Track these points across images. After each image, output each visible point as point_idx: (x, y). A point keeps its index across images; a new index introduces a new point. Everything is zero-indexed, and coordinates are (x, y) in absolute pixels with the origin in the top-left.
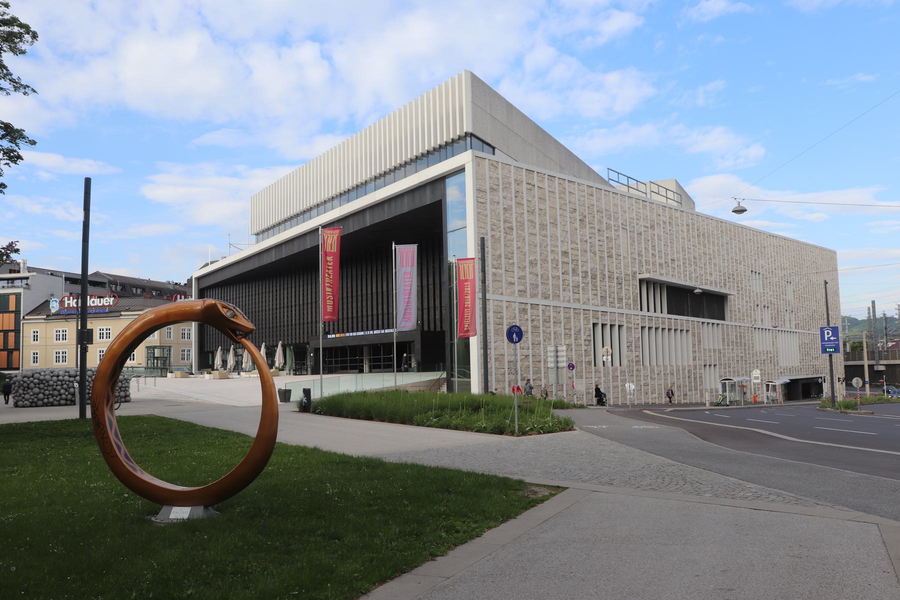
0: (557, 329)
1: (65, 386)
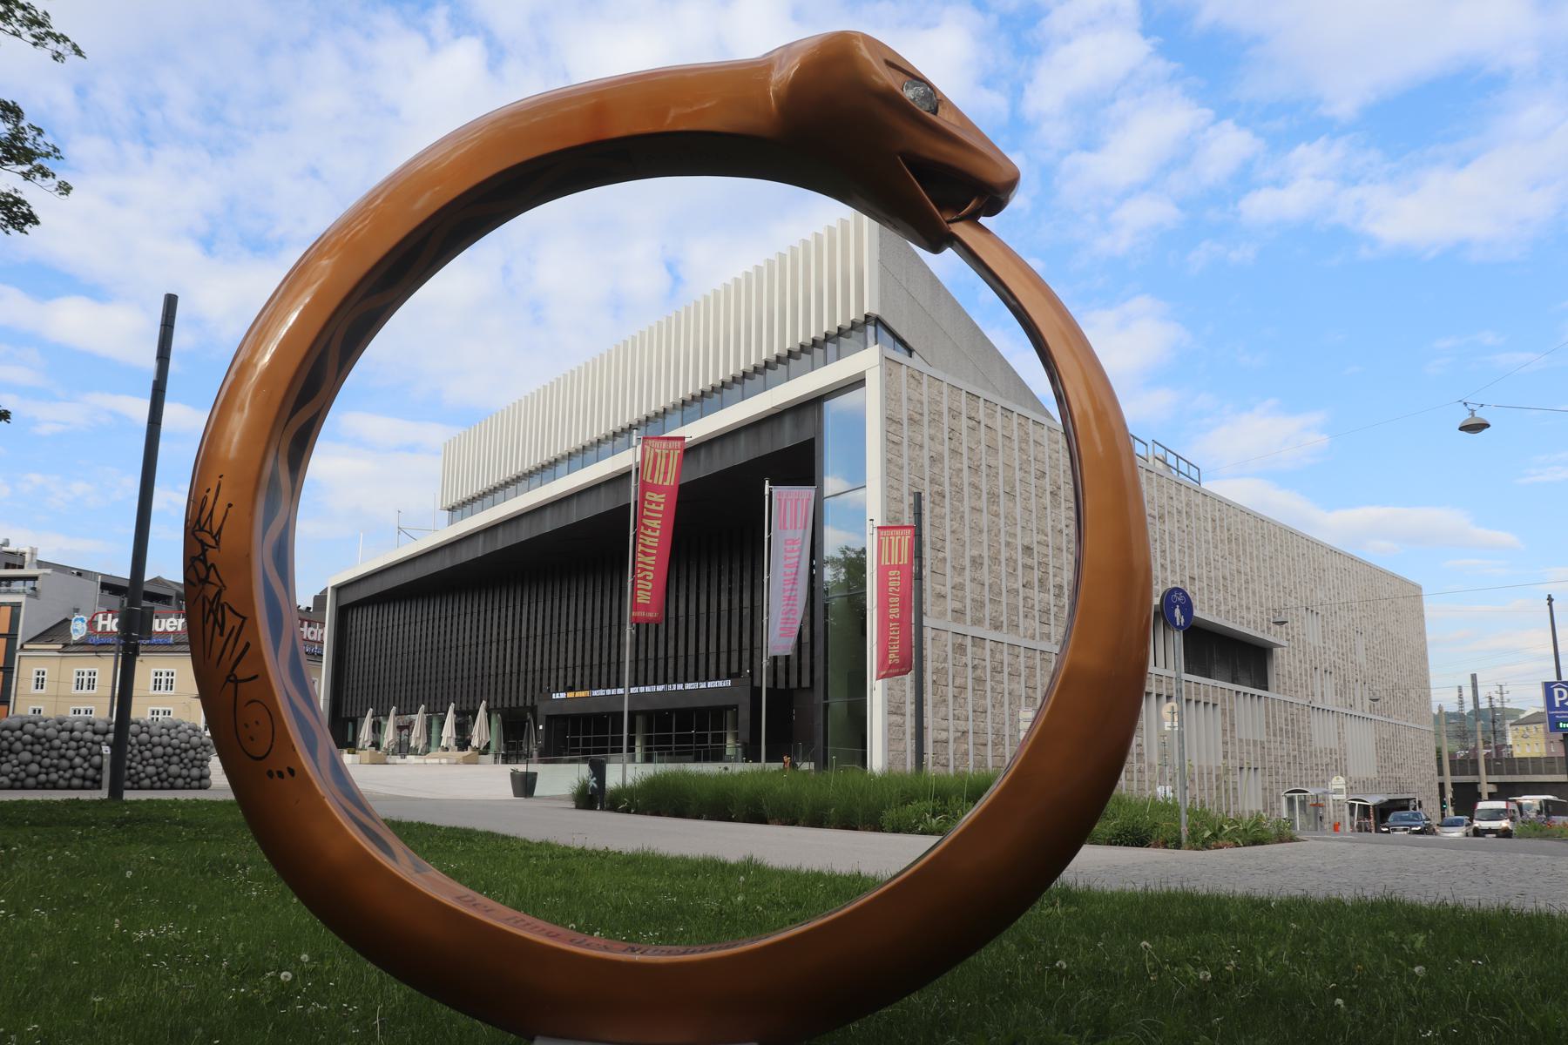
1: (84, 751)
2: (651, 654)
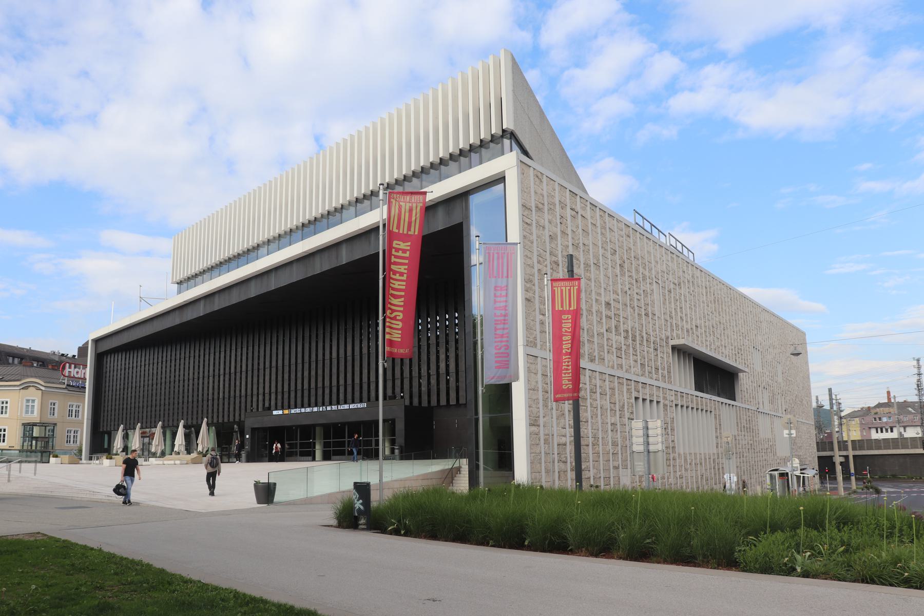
0: (604, 402)
2: (327, 383)
